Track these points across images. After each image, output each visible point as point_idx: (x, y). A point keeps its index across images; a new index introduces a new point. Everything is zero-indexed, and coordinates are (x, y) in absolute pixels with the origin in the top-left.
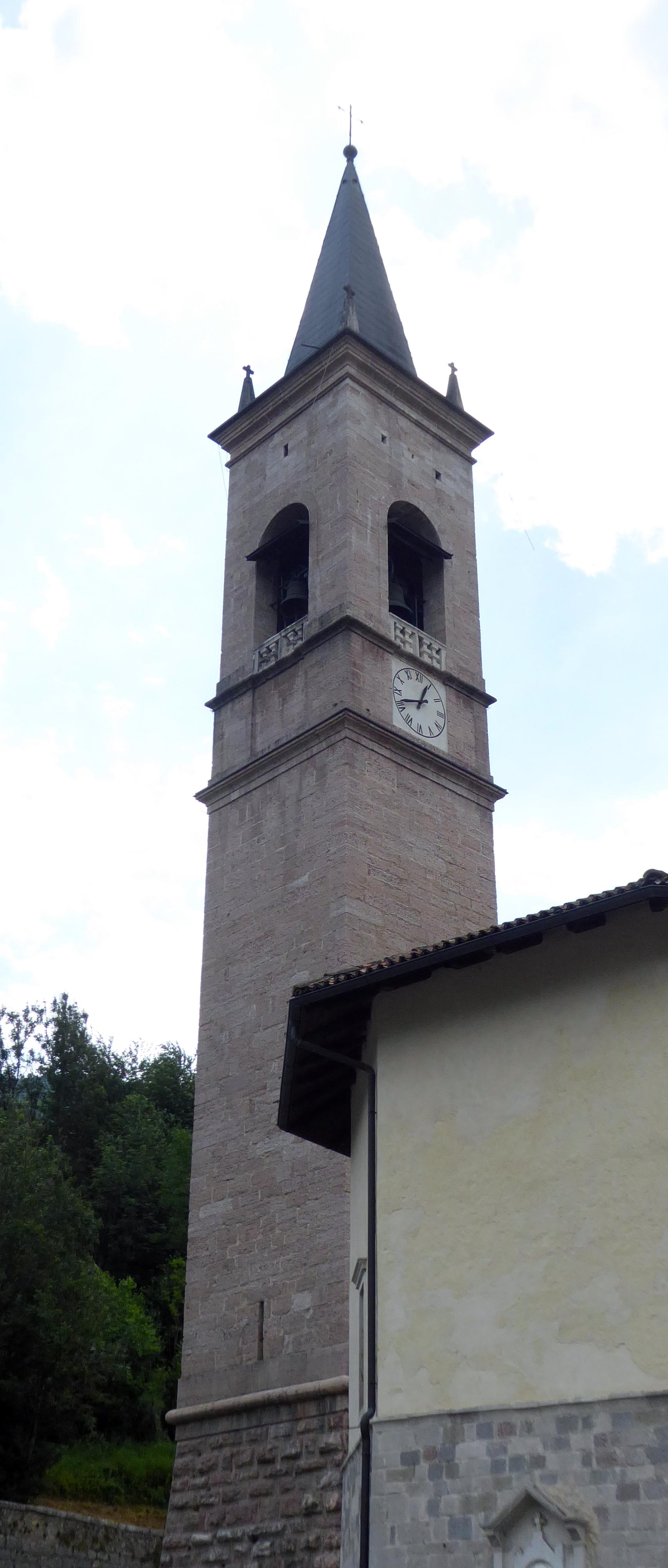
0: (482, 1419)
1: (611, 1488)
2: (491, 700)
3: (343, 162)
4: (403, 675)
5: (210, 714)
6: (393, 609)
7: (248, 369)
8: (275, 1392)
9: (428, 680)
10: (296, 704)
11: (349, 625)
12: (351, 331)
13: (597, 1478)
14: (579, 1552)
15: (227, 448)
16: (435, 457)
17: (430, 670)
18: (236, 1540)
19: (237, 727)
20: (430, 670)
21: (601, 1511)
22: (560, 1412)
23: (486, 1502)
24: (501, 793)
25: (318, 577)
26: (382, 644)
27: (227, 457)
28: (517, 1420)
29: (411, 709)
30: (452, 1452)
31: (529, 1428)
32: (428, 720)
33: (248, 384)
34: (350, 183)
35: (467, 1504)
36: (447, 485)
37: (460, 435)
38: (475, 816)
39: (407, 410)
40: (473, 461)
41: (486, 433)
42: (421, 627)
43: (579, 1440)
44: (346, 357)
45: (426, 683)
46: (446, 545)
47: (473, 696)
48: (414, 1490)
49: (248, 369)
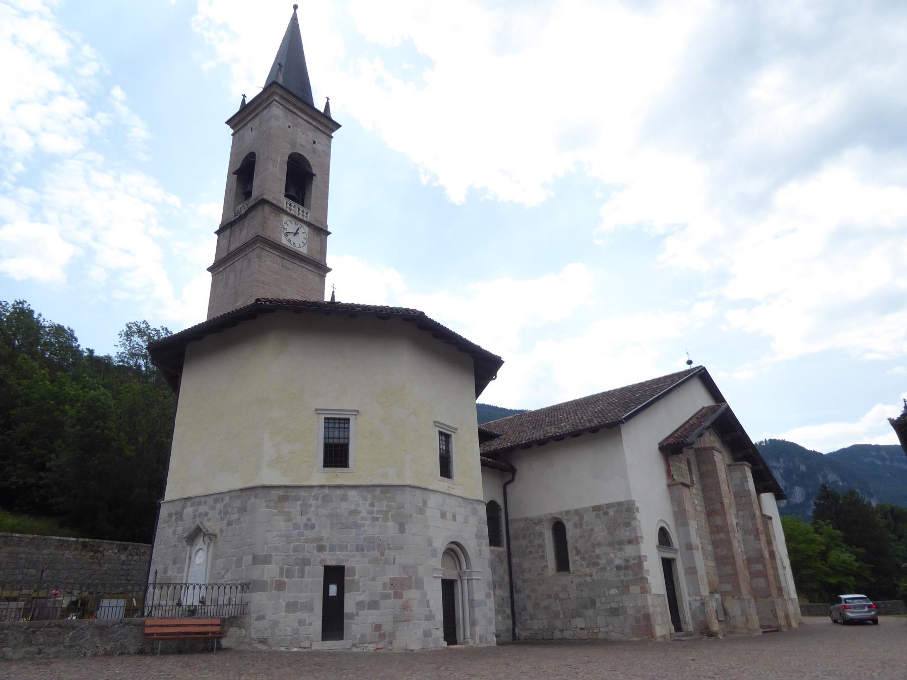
0: (193, 500)
1: (225, 522)
2: (329, 233)
4: (289, 223)
5: (216, 236)
6: (286, 196)
7: (328, 98)
9: (300, 225)
11: (263, 202)
12: (289, 81)
15: (232, 128)
16: (312, 135)
17: (302, 221)
19: (225, 242)
20: (302, 221)
22: (215, 496)
24: (329, 270)
25: (256, 182)
26: (279, 210)
27: (232, 131)
28: (203, 499)
29: (291, 237)
31: (205, 503)
33: (244, 101)
34: (294, 19)
36: (318, 146)
37: (326, 126)
38: (317, 279)
39: (302, 115)
40: (332, 137)
42: (303, 205)
43: (219, 506)
44: (274, 93)
45: (299, 226)
47: (321, 231)
48: (169, 526)
49: (328, 98)
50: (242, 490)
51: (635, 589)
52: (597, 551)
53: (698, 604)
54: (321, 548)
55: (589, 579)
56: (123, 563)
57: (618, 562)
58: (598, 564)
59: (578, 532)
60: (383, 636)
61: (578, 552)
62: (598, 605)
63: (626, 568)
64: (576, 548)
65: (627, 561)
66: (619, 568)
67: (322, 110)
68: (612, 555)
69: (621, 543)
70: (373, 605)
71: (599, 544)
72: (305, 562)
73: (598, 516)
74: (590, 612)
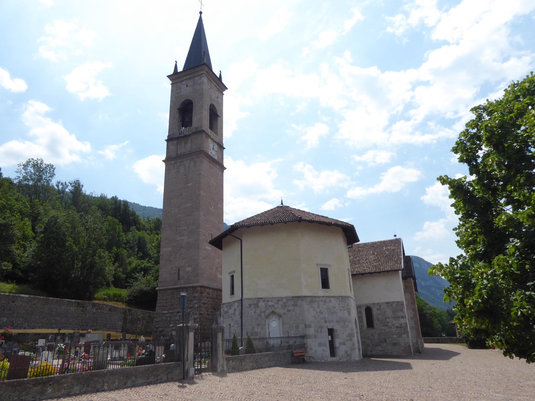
1: (286, 310)
3: (199, 15)
5: (166, 143)
8: (183, 286)
9: (215, 144)
10: (189, 145)
13: (283, 308)
14: (281, 319)
15: (171, 80)
17: (215, 142)
18: (173, 313)
20: (215, 142)
21: (284, 314)
23: (264, 312)
30: (258, 304)
31: (272, 301)
32: (213, 153)
34: (200, 21)
35: (261, 312)
36: (219, 100)
37: (222, 88)
41: (227, 89)
46: (219, 114)
47: (221, 147)
50: (293, 297)
51: (404, 336)
52: (388, 320)
53: (415, 341)
54: (326, 322)
55: (384, 331)
56: (94, 314)
57: (397, 325)
58: (388, 325)
59: (379, 312)
60: (348, 355)
61: (379, 320)
62: (388, 341)
63: (401, 327)
64: (378, 319)
65: (401, 324)
66: (397, 327)
67: (218, 76)
68: (394, 322)
69: (398, 317)
70: (344, 344)
71: (389, 318)
72: (322, 327)
73: (388, 306)
74: (384, 344)
